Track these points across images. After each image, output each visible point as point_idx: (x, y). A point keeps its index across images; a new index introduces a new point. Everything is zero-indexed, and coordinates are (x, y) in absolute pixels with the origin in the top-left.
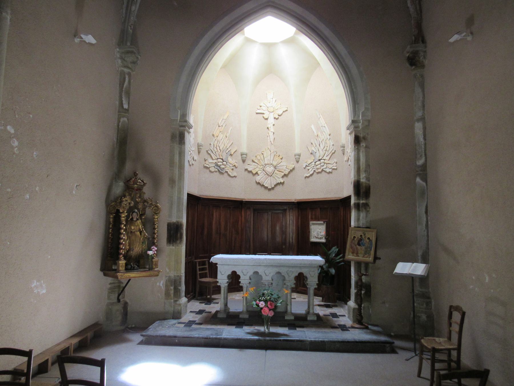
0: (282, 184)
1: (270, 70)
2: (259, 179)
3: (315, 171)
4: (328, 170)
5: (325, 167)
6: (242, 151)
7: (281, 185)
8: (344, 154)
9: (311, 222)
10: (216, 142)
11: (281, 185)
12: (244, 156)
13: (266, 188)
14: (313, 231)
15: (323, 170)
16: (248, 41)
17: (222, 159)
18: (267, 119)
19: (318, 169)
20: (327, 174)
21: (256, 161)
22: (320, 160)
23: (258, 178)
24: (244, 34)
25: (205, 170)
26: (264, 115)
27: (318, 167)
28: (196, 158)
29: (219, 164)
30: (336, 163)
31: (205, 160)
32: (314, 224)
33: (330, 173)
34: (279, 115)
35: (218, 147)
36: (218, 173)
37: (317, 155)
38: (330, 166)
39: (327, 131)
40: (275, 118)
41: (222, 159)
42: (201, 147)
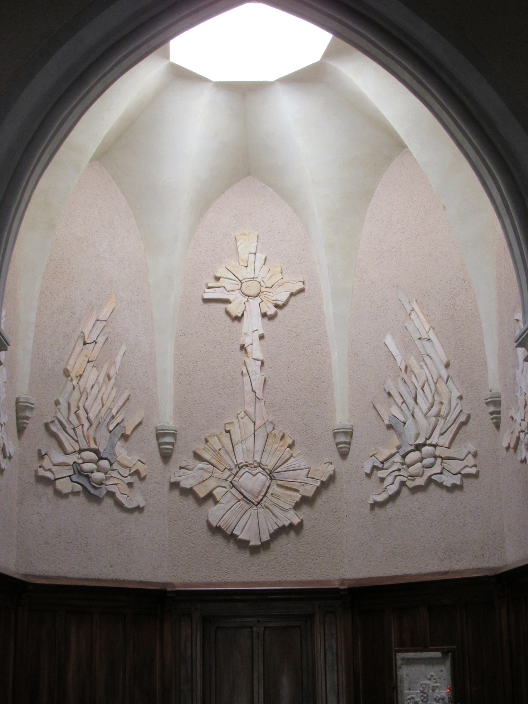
0: (296, 529)
1: (247, 164)
2: (220, 514)
3: (403, 484)
4: (448, 480)
5: (437, 469)
6: (159, 425)
7: (292, 534)
8: (498, 426)
9: (400, 656)
10: (76, 394)
11: (292, 534)
12: (168, 439)
13: (243, 544)
14: (406, 685)
15: (430, 481)
16: (182, 76)
17: (96, 452)
18: (238, 319)
19: (413, 477)
20: (444, 493)
21: (207, 456)
22: (418, 448)
23: (214, 514)
24: (167, 56)
25: (40, 488)
26: (229, 307)
27: (413, 470)
28: (11, 449)
29: (87, 466)
30: (475, 455)
31: (41, 457)
32: (409, 662)
33: (454, 488)
34: (276, 306)
35: (81, 412)
36: (82, 498)
37: (410, 430)
38: (454, 466)
39: (439, 353)
40: (264, 315)
41: (96, 452)
42: (28, 414)
